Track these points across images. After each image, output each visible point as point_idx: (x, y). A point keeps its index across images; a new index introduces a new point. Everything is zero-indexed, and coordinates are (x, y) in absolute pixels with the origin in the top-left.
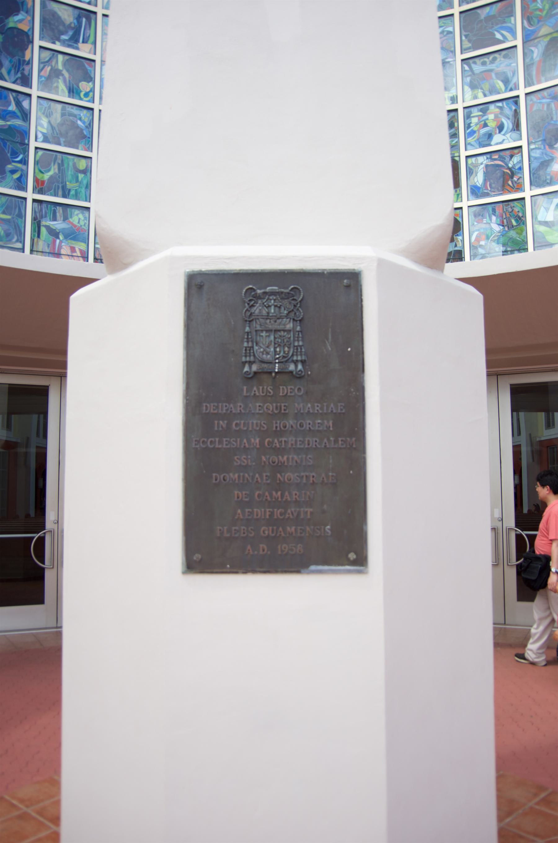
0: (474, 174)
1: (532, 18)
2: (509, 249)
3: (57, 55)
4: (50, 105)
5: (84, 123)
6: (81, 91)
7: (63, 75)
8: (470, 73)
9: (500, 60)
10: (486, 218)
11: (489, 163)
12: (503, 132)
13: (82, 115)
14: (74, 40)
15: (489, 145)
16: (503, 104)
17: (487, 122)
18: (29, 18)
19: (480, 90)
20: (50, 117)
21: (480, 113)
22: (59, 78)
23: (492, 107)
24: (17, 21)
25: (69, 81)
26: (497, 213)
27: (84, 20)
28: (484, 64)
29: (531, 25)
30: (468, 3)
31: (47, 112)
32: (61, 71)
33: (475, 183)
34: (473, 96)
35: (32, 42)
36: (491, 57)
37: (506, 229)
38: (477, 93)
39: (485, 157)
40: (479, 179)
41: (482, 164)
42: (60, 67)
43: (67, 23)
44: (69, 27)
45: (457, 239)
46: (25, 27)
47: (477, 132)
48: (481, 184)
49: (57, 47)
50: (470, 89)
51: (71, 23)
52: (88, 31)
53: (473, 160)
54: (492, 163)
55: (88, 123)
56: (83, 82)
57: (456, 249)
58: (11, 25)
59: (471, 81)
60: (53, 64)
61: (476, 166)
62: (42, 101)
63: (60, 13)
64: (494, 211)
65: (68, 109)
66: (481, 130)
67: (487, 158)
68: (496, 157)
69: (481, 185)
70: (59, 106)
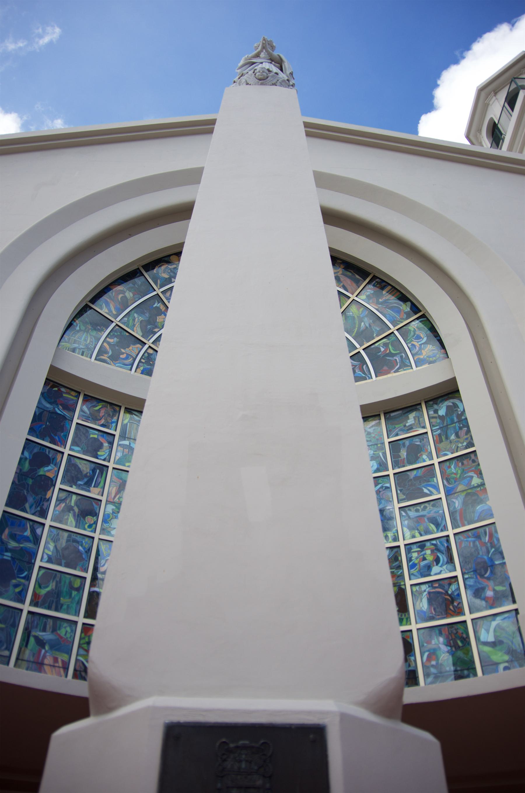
1: (450, 479)
5: (84, 548)
6: (86, 523)
7: (73, 510)
9: (430, 508)
12: (440, 565)
13: (84, 542)
15: (429, 575)
17: (425, 556)
18: (56, 469)
19: (416, 531)
21: (419, 549)
22: (70, 513)
24: (46, 471)
27: (98, 471)
28: (417, 511)
29: (450, 484)
30: (399, 468)
31: (55, 539)
32: (73, 507)
33: (421, 608)
34: (411, 535)
35: (55, 486)
37: (454, 649)
38: (415, 533)
39: (427, 586)
41: (425, 591)
45: (410, 659)
46: (51, 475)
47: (418, 565)
50: (408, 530)
51: (87, 473)
52: (100, 479)
54: (434, 590)
56: (89, 517)
57: (410, 668)
59: (408, 524)
61: (421, 593)
63: (80, 466)
65: (73, 537)
66: (421, 563)
67: (429, 586)
68: (437, 585)
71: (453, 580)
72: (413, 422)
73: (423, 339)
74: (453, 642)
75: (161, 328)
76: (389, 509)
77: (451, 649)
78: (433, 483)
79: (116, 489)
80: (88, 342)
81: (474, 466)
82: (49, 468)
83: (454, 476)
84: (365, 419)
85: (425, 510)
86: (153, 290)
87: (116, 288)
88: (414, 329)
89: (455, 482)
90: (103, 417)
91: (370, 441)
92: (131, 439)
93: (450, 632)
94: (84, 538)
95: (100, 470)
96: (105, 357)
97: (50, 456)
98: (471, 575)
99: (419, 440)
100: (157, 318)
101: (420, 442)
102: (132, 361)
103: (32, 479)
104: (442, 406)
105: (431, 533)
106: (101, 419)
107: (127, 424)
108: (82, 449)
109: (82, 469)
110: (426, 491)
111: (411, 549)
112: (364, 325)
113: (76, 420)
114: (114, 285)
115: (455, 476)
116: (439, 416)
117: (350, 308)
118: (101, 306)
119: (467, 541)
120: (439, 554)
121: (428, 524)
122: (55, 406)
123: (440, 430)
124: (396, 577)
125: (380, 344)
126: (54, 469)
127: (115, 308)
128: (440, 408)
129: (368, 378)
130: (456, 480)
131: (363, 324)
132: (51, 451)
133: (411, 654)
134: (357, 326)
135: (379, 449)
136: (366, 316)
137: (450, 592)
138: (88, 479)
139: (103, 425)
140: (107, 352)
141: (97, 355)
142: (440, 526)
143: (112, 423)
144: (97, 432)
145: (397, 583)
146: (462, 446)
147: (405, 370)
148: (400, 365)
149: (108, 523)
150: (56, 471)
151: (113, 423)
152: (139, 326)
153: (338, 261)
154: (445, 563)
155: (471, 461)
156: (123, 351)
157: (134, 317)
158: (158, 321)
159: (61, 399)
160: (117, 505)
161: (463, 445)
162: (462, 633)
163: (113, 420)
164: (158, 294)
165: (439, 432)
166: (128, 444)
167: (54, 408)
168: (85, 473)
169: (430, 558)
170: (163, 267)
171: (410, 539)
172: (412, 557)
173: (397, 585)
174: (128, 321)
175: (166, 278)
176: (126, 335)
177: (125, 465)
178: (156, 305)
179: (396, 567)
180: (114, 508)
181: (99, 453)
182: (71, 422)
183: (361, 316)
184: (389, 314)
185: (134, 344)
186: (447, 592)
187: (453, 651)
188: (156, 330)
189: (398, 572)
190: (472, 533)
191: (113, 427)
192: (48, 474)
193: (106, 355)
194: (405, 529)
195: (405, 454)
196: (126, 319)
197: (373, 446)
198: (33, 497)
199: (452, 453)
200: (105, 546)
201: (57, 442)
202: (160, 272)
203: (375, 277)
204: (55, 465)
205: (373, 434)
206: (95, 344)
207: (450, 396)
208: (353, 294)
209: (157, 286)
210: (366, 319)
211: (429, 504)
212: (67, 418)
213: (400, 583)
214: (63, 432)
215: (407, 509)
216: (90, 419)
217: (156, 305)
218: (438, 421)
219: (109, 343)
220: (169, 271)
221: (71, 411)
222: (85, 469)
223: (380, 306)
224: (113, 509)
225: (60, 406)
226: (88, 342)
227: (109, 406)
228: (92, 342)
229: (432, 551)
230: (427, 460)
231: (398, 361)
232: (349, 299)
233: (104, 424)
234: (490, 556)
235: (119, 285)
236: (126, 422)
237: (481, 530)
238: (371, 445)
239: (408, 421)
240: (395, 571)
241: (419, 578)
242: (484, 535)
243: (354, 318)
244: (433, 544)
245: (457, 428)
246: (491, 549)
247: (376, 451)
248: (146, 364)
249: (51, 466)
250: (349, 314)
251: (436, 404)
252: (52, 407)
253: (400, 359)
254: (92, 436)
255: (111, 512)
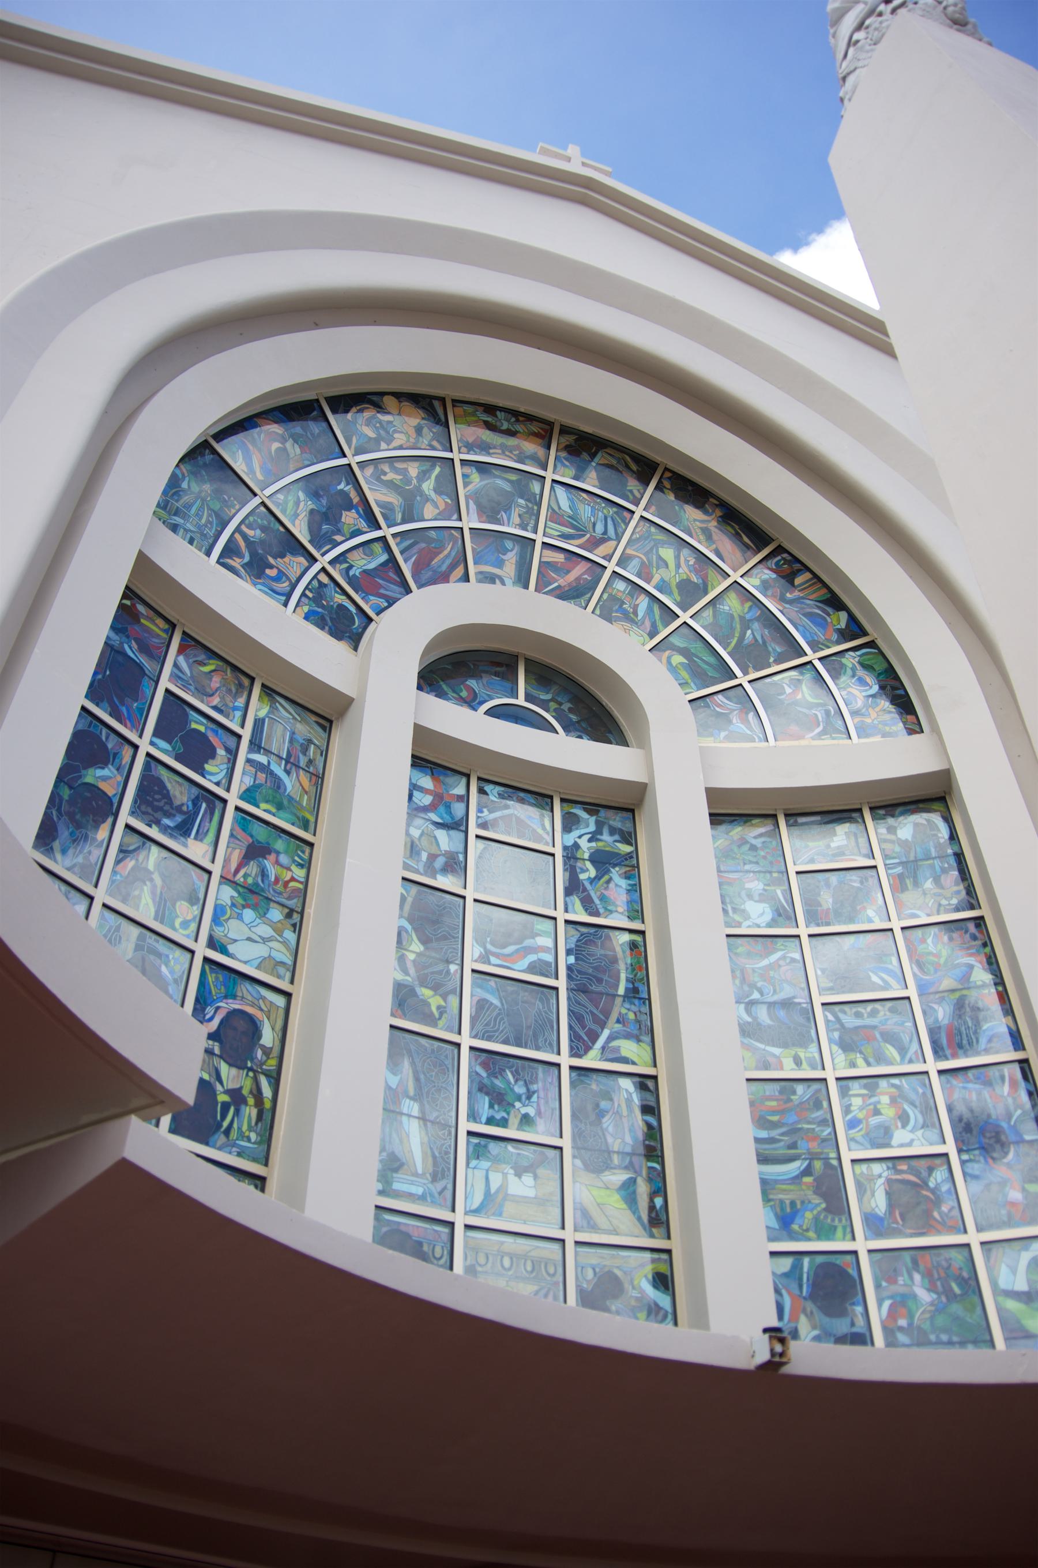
0: (869, 1192)
1: (924, 965)
2: (955, 1339)
3: (150, 846)
4: (120, 924)
5: (172, 972)
6: (177, 916)
7: (152, 880)
8: (838, 1026)
9: (885, 1015)
10: (903, 1276)
11: (894, 1177)
12: (910, 1127)
13: (171, 957)
14: (183, 830)
15: (887, 1145)
16: (901, 1081)
17: (879, 1106)
18: (120, 779)
19: (858, 1055)
20: (115, 945)
21: (864, 1092)
22: (146, 885)
23: (883, 1083)
24: (99, 777)
25: (161, 892)
26: (922, 1267)
27: (204, 805)
28: (858, 1015)
29: (925, 972)
30: (818, 925)
31: (112, 936)
32: (152, 873)
33: (873, 1210)
34: (848, 1062)
35: (116, 816)
36: (870, 1007)
37: (944, 1299)
38: (856, 1058)
39: (884, 1166)
40: (879, 1203)
41: (880, 1176)
42: (151, 866)
43: (177, 803)
44: (179, 809)
45: (853, 1310)
46: (110, 789)
47: (864, 1122)
48: (883, 1211)
49: (153, 832)
50: (840, 1051)
51: (183, 805)
52: (207, 824)
53: (864, 1167)
54: (898, 1177)
55: (179, 974)
56: (183, 902)
57: (855, 1330)
58: (89, 779)
59: (840, 1037)
60: (141, 857)
61: (871, 1179)
62: (108, 914)
63: (169, 786)
64: (915, 1262)
65: (148, 940)
66: (870, 1120)
67: (888, 1168)
68: (904, 1167)
69: (885, 1214)
70: (135, 931)
71: (938, 1161)
72: (845, 842)
73: (871, 687)
74: (943, 1286)
75: (348, 537)
76: (800, 1004)
77: (939, 1298)
78: (890, 967)
79: (240, 852)
80: (203, 521)
81: (975, 946)
82: (105, 772)
83: (931, 958)
84: (716, 818)
85: (875, 1017)
86: (341, 455)
87: (268, 427)
88: (853, 664)
89: (936, 971)
90: (216, 690)
91: (757, 863)
92: (272, 753)
93: (935, 1264)
94: (172, 949)
95: (208, 806)
96: (236, 563)
97: (110, 746)
98: (974, 1155)
99: (859, 879)
100: (342, 514)
101: (862, 882)
102: (288, 589)
103: (71, 788)
104: (905, 821)
105: (890, 1063)
106: (212, 695)
107: (263, 720)
108: (174, 749)
109: (171, 792)
110: (875, 979)
111: (848, 1089)
112: (751, 636)
113: (165, 683)
114: (265, 418)
115: (936, 960)
116: (899, 839)
117: (725, 596)
118: (234, 453)
119: (964, 1088)
120: (906, 1106)
121: (882, 1044)
122: (124, 639)
123: (901, 868)
124: (820, 1141)
125: (783, 678)
126: (115, 776)
127: (261, 468)
128: (902, 825)
129: (757, 740)
130: (937, 967)
131: (749, 632)
132: (113, 736)
133: (855, 1300)
134: (737, 635)
135: (776, 882)
136: (758, 619)
137: (932, 1184)
138: (184, 817)
139: (215, 708)
140: (240, 555)
141: (221, 556)
142: (906, 1052)
143: (235, 708)
144: (204, 721)
145: (821, 1153)
146: (949, 904)
147: (834, 739)
148: (824, 727)
149: (223, 925)
150: (118, 783)
151: (237, 710)
152: (306, 519)
153: (712, 500)
154: (920, 1126)
155: (968, 935)
156: (271, 560)
157: (298, 498)
158: (343, 520)
159: (137, 628)
160: (241, 890)
161: (951, 902)
162: (961, 1269)
163: (236, 704)
164: (349, 465)
165: (899, 870)
166: (266, 763)
167: (122, 643)
168: (177, 803)
169: (888, 1113)
170: (367, 414)
171: (844, 1068)
172: (850, 1105)
173: (822, 1157)
174: (286, 502)
175: (370, 438)
176: (279, 530)
177: (258, 807)
178: (341, 487)
179: (818, 1120)
180: (235, 894)
181: (207, 767)
182: (154, 684)
183: (748, 617)
184: (804, 627)
185: (293, 554)
186: (926, 1184)
187: (942, 1302)
188: (338, 538)
189: (823, 1131)
190: (974, 1075)
191: (236, 719)
192: (104, 786)
193: (238, 560)
194: (835, 1048)
195: (831, 900)
196: (280, 496)
197: (762, 875)
198: (71, 830)
199: (928, 915)
200: (214, 975)
201: (125, 719)
202: (360, 423)
203: (780, 550)
204: (118, 770)
205: (763, 850)
206: (216, 530)
207: (921, 805)
208: (735, 571)
209: (350, 447)
210: (756, 626)
211: (884, 1006)
212: (147, 672)
213: (828, 1154)
214: (137, 701)
215: (837, 1008)
216: (192, 688)
217: (341, 487)
218: (897, 849)
219: (245, 537)
220: (378, 425)
221: (154, 658)
222: (177, 793)
223: (787, 606)
224: (232, 897)
225: (133, 642)
226: (203, 521)
227: (229, 671)
228: (211, 523)
229: (893, 1101)
230: (876, 919)
231: (820, 719)
232: (726, 579)
233: (219, 706)
234: (1012, 1123)
235: (276, 422)
236: (262, 713)
237: (993, 1072)
238: (759, 872)
239: (835, 839)
240: (817, 1129)
241: (867, 1149)
242: (999, 1081)
243: (732, 617)
244: (893, 1086)
245: (938, 868)
246: (1016, 1110)
247: (768, 885)
248: (314, 602)
249: (109, 769)
250: (721, 607)
251: (893, 816)
252: (118, 639)
253: (824, 715)
254: (194, 726)
255: (229, 903)
